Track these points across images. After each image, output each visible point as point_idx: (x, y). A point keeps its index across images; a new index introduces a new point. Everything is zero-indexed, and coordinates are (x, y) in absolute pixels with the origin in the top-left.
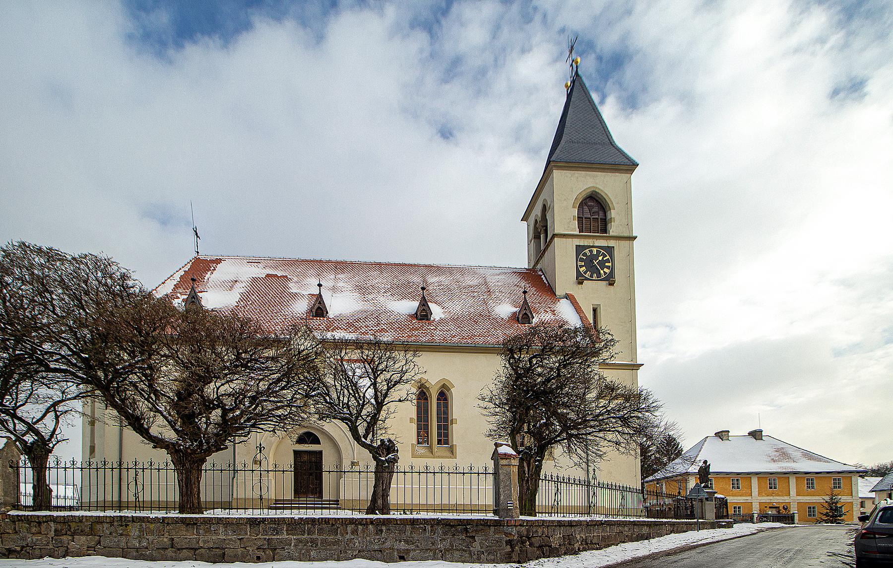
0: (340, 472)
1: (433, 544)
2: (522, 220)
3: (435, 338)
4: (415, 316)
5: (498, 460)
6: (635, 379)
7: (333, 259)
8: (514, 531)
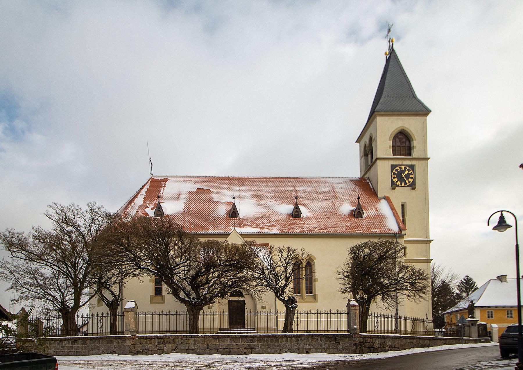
0: (255, 314)
1: (321, 346)
2: (356, 142)
3: (304, 230)
4: (291, 215)
5: (350, 307)
6: (428, 251)
7: (236, 176)
8: (357, 339)
